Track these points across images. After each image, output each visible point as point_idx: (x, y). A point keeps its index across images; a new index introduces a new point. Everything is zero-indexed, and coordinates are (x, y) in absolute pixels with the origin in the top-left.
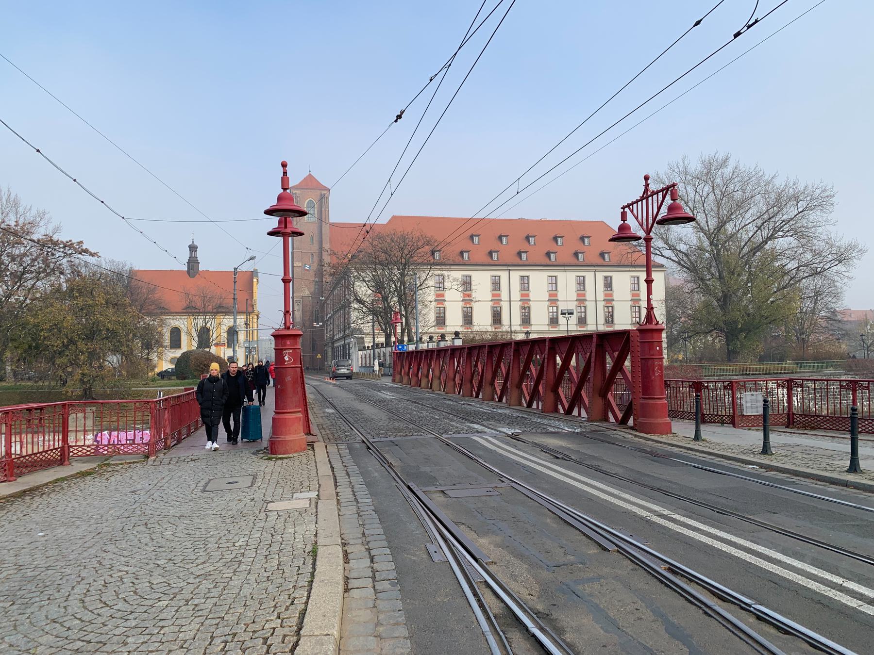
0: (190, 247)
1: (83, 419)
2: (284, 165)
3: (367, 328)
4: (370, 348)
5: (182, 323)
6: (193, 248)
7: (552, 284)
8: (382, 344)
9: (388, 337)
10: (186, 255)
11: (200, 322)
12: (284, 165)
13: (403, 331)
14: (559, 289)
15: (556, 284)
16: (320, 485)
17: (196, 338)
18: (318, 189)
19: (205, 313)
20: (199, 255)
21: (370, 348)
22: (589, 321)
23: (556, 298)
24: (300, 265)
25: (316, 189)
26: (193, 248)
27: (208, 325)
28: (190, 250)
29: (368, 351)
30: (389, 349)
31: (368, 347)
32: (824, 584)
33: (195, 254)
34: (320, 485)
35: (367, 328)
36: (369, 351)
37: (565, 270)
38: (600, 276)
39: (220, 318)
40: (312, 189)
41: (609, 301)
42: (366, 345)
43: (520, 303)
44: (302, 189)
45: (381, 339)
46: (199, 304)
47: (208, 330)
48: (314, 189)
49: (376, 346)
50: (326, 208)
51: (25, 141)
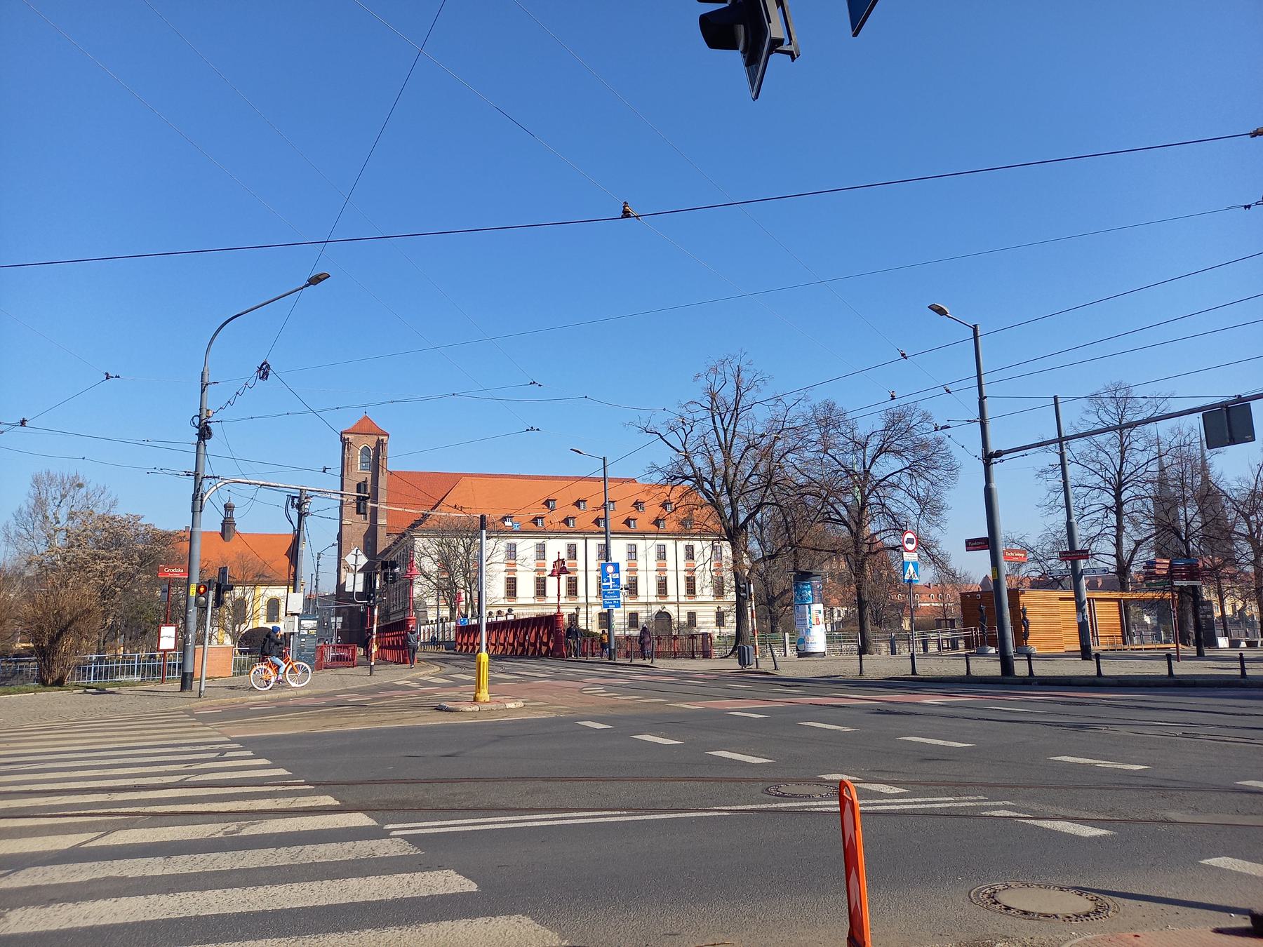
2: (559, 553)
3: (431, 602)
4: (434, 622)
7: (511, 551)
8: (447, 618)
9: (452, 610)
12: (559, 553)
13: (467, 607)
14: (638, 558)
15: (635, 552)
16: (659, 434)
18: (376, 434)
20: (236, 514)
21: (434, 622)
22: (669, 592)
25: (372, 434)
29: (432, 626)
30: (453, 624)
31: (432, 621)
33: (231, 515)
34: (659, 434)
35: (431, 602)
36: (433, 626)
37: (645, 539)
38: (681, 545)
39: (261, 590)
40: (368, 434)
41: (662, 570)
42: (430, 619)
44: (356, 434)
45: (445, 612)
48: (371, 434)
49: (441, 620)
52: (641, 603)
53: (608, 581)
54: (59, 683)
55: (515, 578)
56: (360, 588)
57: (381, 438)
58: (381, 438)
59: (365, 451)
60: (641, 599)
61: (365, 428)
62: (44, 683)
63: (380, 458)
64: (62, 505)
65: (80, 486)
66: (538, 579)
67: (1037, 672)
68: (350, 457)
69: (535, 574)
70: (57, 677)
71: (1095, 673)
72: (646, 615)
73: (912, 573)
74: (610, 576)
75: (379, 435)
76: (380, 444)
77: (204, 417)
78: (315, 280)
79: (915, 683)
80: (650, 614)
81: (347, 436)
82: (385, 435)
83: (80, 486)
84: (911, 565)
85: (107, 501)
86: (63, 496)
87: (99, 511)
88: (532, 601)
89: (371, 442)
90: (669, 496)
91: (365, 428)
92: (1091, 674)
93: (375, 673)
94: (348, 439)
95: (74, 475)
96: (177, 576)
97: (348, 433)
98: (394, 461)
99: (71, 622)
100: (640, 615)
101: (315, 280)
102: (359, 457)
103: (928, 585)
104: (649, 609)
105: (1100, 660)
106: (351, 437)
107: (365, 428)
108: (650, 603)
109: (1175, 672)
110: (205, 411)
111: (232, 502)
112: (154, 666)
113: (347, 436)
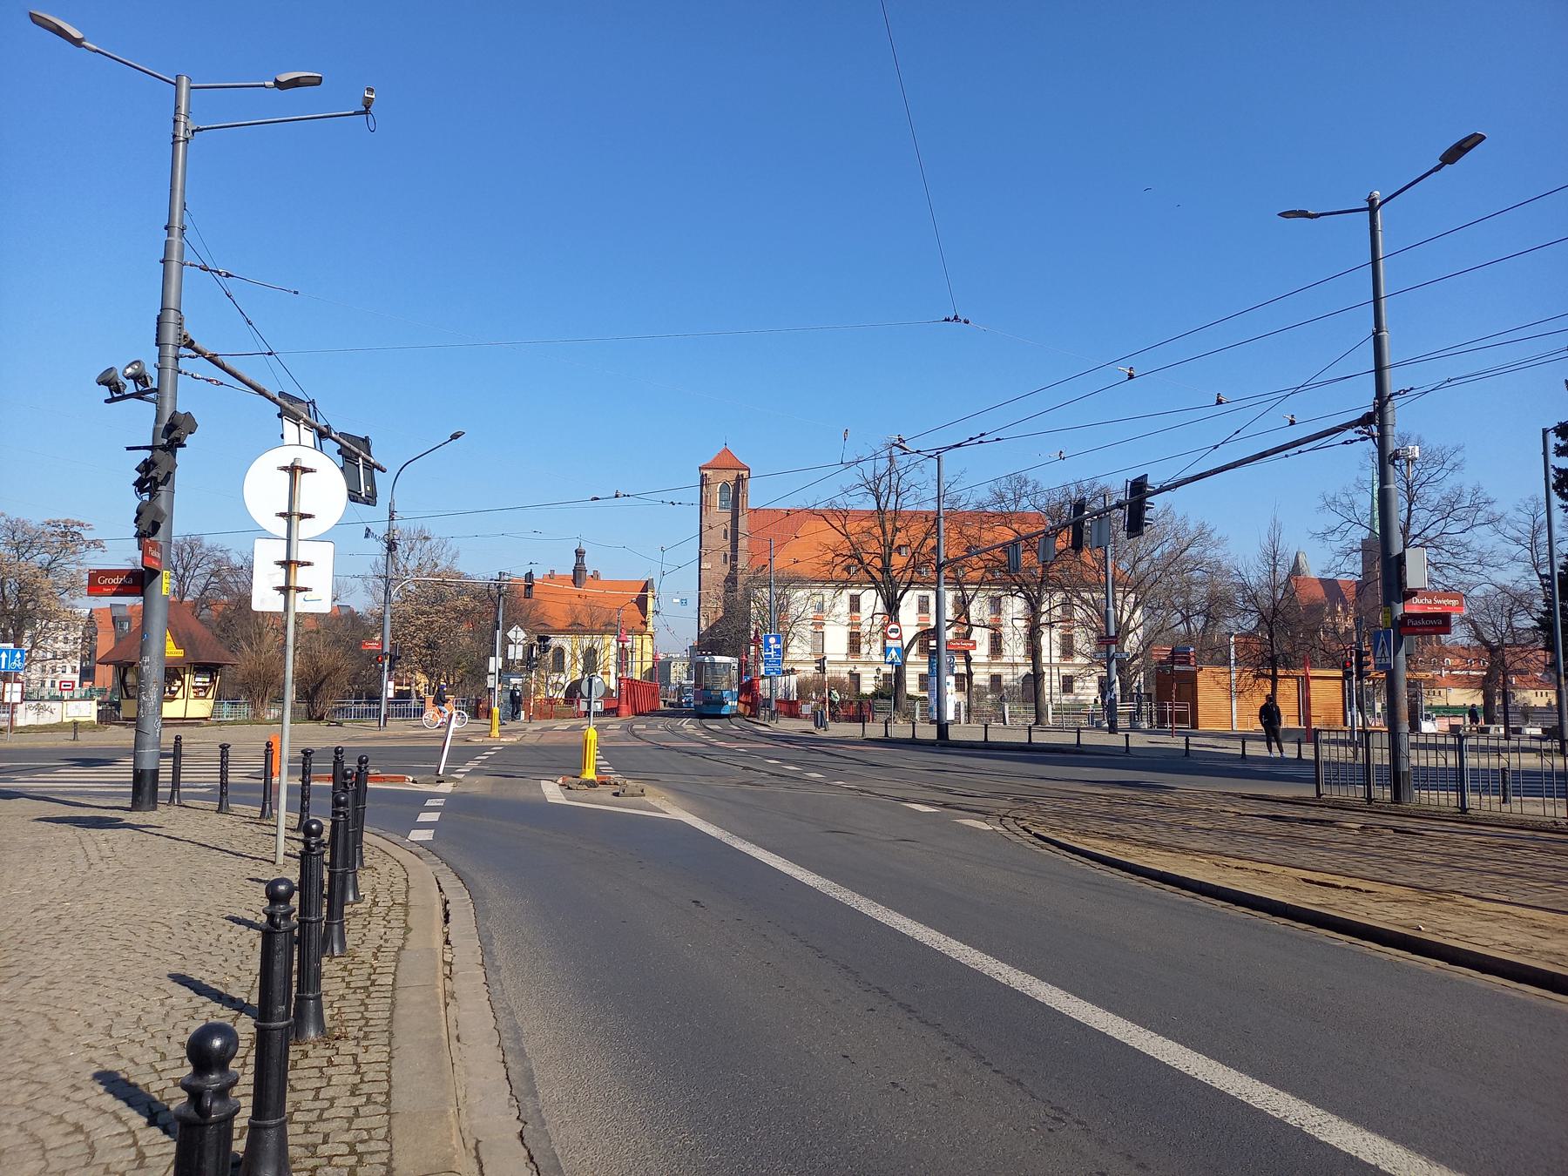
0: (576, 551)
1: (296, 1077)
5: (565, 643)
6: (579, 554)
10: (572, 560)
11: (586, 641)
17: (582, 661)
18: (735, 469)
19: (591, 632)
23: (148, 775)
24: (709, 567)
26: (579, 554)
27: (596, 645)
28: (577, 556)
32: (1040, 839)
33: (582, 560)
43: (849, 629)
46: (586, 621)
47: (595, 651)
50: (744, 493)
51: (395, 482)
52: (1006, 664)
53: (770, 651)
54: (321, 718)
55: (823, 632)
56: (520, 656)
57: (741, 472)
58: (741, 472)
59: (725, 485)
60: (1005, 660)
61: (727, 463)
62: (310, 718)
63: (740, 495)
64: (410, 558)
65: (426, 538)
66: (851, 634)
67: (989, 739)
68: (709, 495)
69: (849, 629)
70: (318, 715)
71: (1027, 741)
72: (1011, 677)
73: (894, 656)
74: (772, 647)
75: (738, 469)
76: (740, 480)
77: (391, 535)
78: (455, 436)
79: (887, 742)
80: (1016, 677)
81: (705, 472)
82: (746, 470)
83: (426, 538)
84: (893, 649)
85: (450, 553)
86: (412, 549)
87: (443, 564)
88: (844, 658)
89: (730, 476)
90: (831, 574)
91: (725, 462)
92: (932, 738)
93: (533, 721)
94: (706, 475)
95: (419, 529)
96: (375, 648)
97: (706, 468)
98: (757, 496)
99: (325, 677)
100: (1004, 677)
101: (455, 436)
102: (718, 495)
103: (1466, 646)
104: (1015, 671)
105: (1283, 744)
106: (709, 472)
107: (725, 462)
108: (1017, 664)
109: (989, 739)
110: (392, 532)
111: (583, 547)
112: (366, 710)
113: (705, 472)
